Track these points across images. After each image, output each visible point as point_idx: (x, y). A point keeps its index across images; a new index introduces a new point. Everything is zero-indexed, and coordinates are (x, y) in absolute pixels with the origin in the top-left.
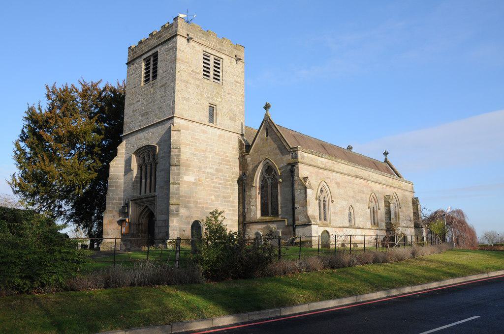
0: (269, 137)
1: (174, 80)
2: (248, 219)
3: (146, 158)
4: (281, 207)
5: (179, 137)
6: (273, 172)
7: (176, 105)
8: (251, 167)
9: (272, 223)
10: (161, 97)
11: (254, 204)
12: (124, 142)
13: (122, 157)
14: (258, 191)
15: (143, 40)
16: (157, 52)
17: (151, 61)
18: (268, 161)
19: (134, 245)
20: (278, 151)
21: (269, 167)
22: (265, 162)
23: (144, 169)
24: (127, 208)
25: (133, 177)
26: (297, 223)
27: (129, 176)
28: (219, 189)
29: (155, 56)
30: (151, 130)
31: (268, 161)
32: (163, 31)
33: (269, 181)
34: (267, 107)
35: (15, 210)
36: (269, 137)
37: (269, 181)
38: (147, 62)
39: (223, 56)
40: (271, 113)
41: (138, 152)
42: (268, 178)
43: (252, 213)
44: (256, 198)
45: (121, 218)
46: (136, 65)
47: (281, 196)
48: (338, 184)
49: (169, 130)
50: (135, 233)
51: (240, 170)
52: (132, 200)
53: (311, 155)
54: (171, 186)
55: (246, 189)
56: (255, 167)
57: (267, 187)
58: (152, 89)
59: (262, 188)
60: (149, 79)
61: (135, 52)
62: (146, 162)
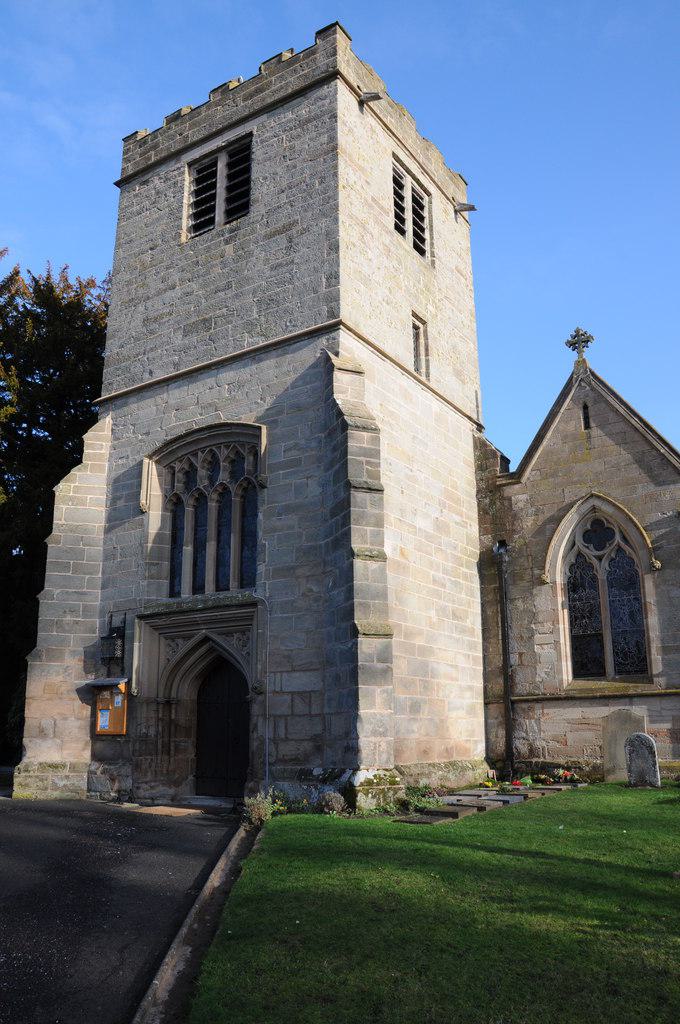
0: (595, 431)
1: (330, 210)
2: (522, 686)
3: (202, 473)
4: (665, 650)
5: (361, 394)
6: (618, 538)
7: (342, 288)
8: (528, 523)
9: (627, 700)
10: (273, 268)
11: (551, 638)
12: (106, 423)
13: (101, 468)
14: (560, 598)
15: (186, 111)
16: (250, 134)
18: (597, 503)
19: (149, 777)
20: (635, 472)
21: (597, 523)
22: (588, 506)
23: (189, 510)
24: (119, 642)
25: (145, 536)
27: (127, 534)
28: (444, 586)
29: (241, 155)
30: (228, 375)
31: (597, 503)
32: (271, 74)
33: (602, 570)
34: (579, 341)
36: (595, 431)
37: (602, 570)
38: (199, 172)
40: (593, 357)
41: (166, 453)
42: (600, 559)
43: (541, 673)
44: (556, 621)
45: (90, 679)
46: (157, 182)
47: (661, 612)
49: (325, 369)
50: (152, 732)
51: (483, 531)
52: (141, 617)
54: (358, 563)
55: (513, 592)
56: (545, 524)
58: (229, 249)
59: (573, 587)
60: (212, 221)
61: (155, 147)
62: (202, 482)
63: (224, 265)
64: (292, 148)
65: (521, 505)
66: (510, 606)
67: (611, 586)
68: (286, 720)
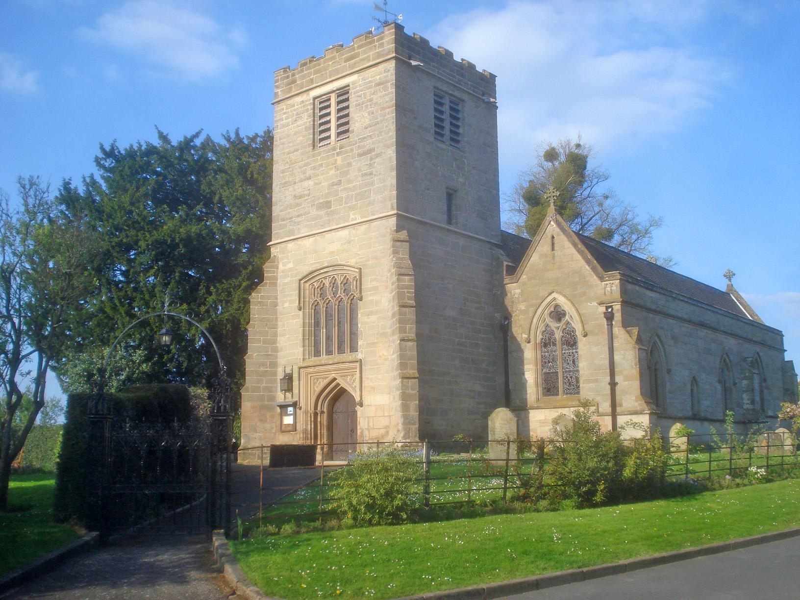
17: (333, 109)
26: (618, 409)
33: (558, 335)
35: (153, 584)
37: (558, 335)
39: (465, 97)
48: (675, 338)
53: (637, 288)
57: (554, 344)
63: (337, 168)
64: (371, 100)
65: (516, 296)
66: (510, 356)
67: (563, 344)
68: (508, 444)
